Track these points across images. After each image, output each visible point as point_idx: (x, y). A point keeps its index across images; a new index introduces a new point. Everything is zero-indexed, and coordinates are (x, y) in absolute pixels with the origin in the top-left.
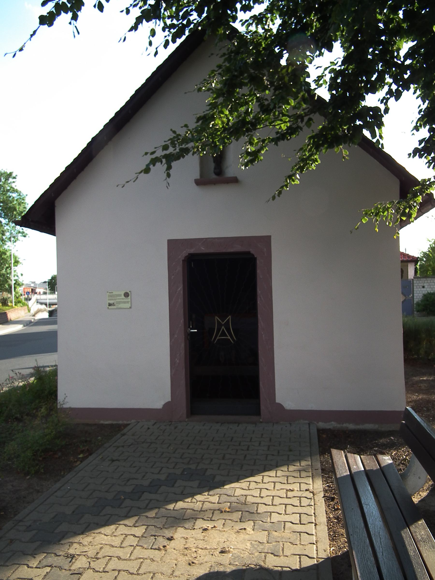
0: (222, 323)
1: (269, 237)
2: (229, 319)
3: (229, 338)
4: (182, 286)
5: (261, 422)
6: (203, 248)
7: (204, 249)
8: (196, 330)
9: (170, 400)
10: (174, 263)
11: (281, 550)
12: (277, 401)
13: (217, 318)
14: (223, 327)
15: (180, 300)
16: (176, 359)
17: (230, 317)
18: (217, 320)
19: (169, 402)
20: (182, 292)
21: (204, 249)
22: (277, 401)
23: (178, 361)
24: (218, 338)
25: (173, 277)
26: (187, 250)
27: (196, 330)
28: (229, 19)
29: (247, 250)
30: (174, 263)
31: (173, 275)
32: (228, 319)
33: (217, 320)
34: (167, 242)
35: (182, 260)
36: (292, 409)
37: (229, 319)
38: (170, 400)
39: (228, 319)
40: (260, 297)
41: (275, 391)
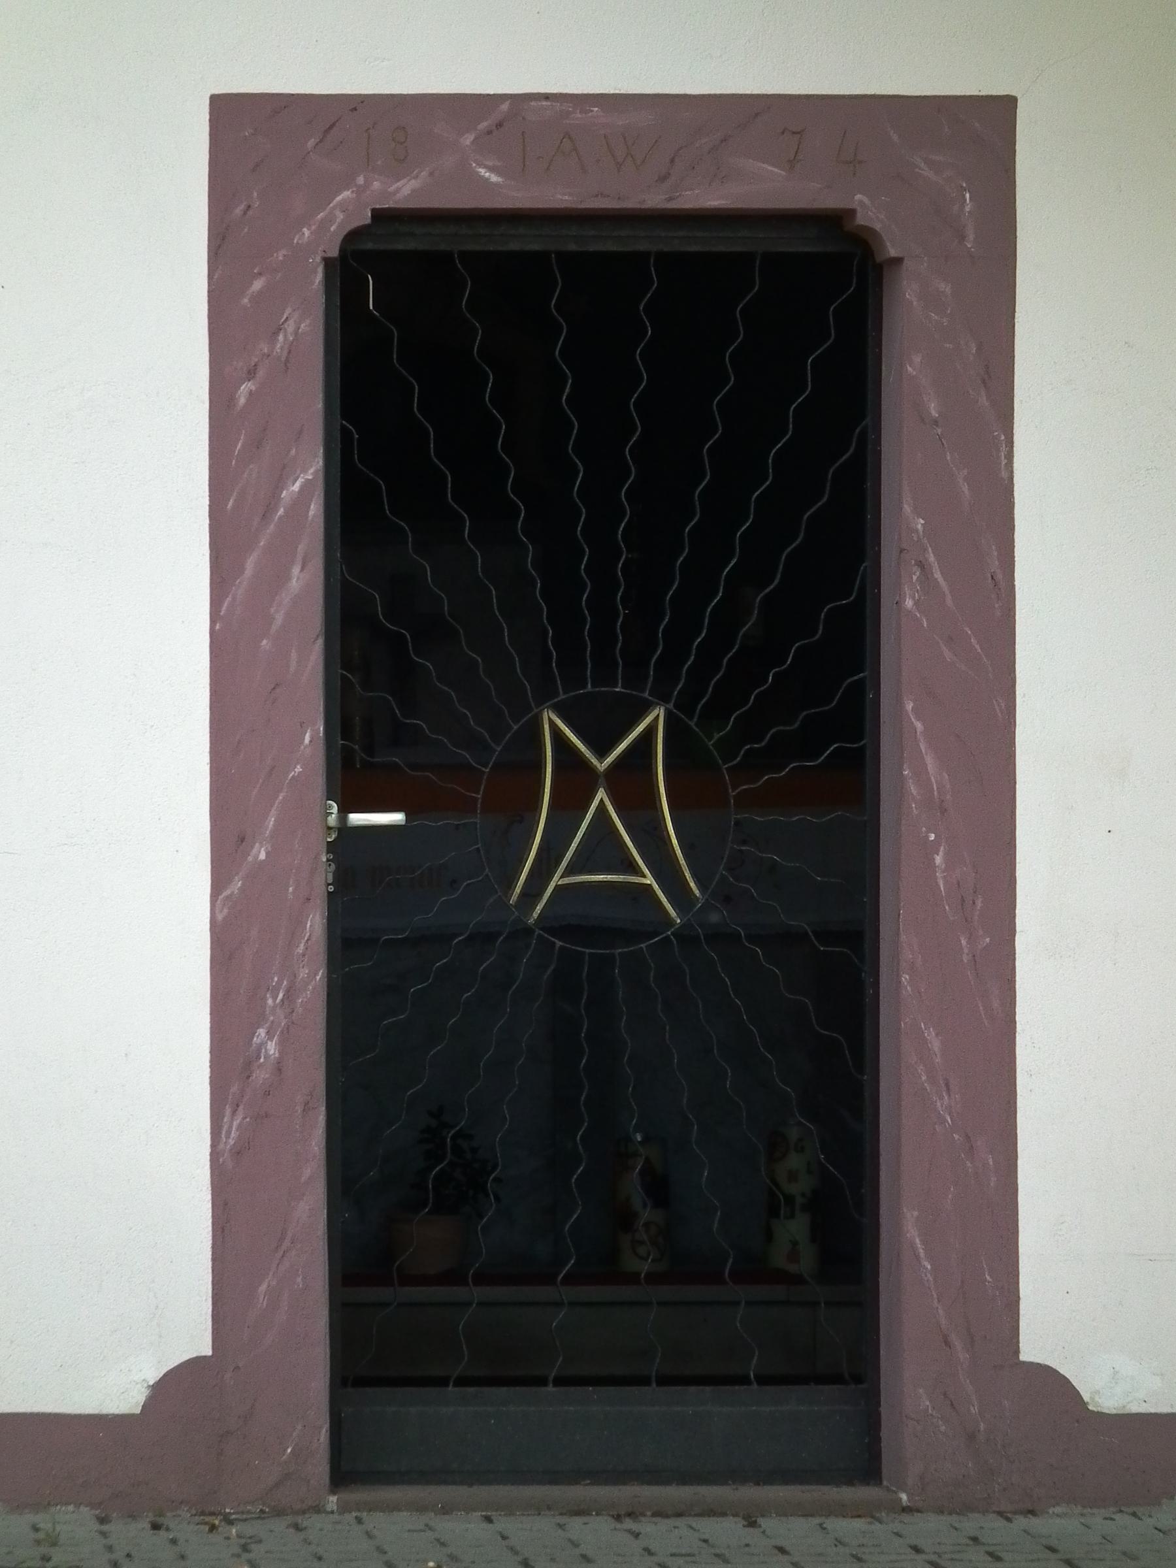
0: (594, 761)
1: (1006, 106)
2: (649, 735)
3: (649, 880)
4: (319, 463)
5: (906, 1510)
6: (491, 169)
7: (494, 178)
8: (395, 818)
9: (204, 1347)
10: (258, 285)
11: (945, 443)
12: (1031, 1350)
13: (550, 719)
14: (601, 794)
15: (296, 570)
16: (262, 1032)
17: (658, 714)
18: (559, 739)
19: (194, 1365)
20: (315, 509)
21: (494, 178)
22: (1031, 1350)
23: (272, 1048)
24: (556, 880)
25: (245, 388)
26: (361, 180)
27: (395, 818)
28: (937, 415)
29: (829, 201)
30: (258, 285)
31: (251, 374)
32: (641, 728)
33: (557, 735)
34: (208, 102)
35: (328, 262)
36: (1135, 1408)
37: (650, 731)
38: (204, 1347)
39: (641, 728)
40: (921, 565)
41: (1014, 1274)
